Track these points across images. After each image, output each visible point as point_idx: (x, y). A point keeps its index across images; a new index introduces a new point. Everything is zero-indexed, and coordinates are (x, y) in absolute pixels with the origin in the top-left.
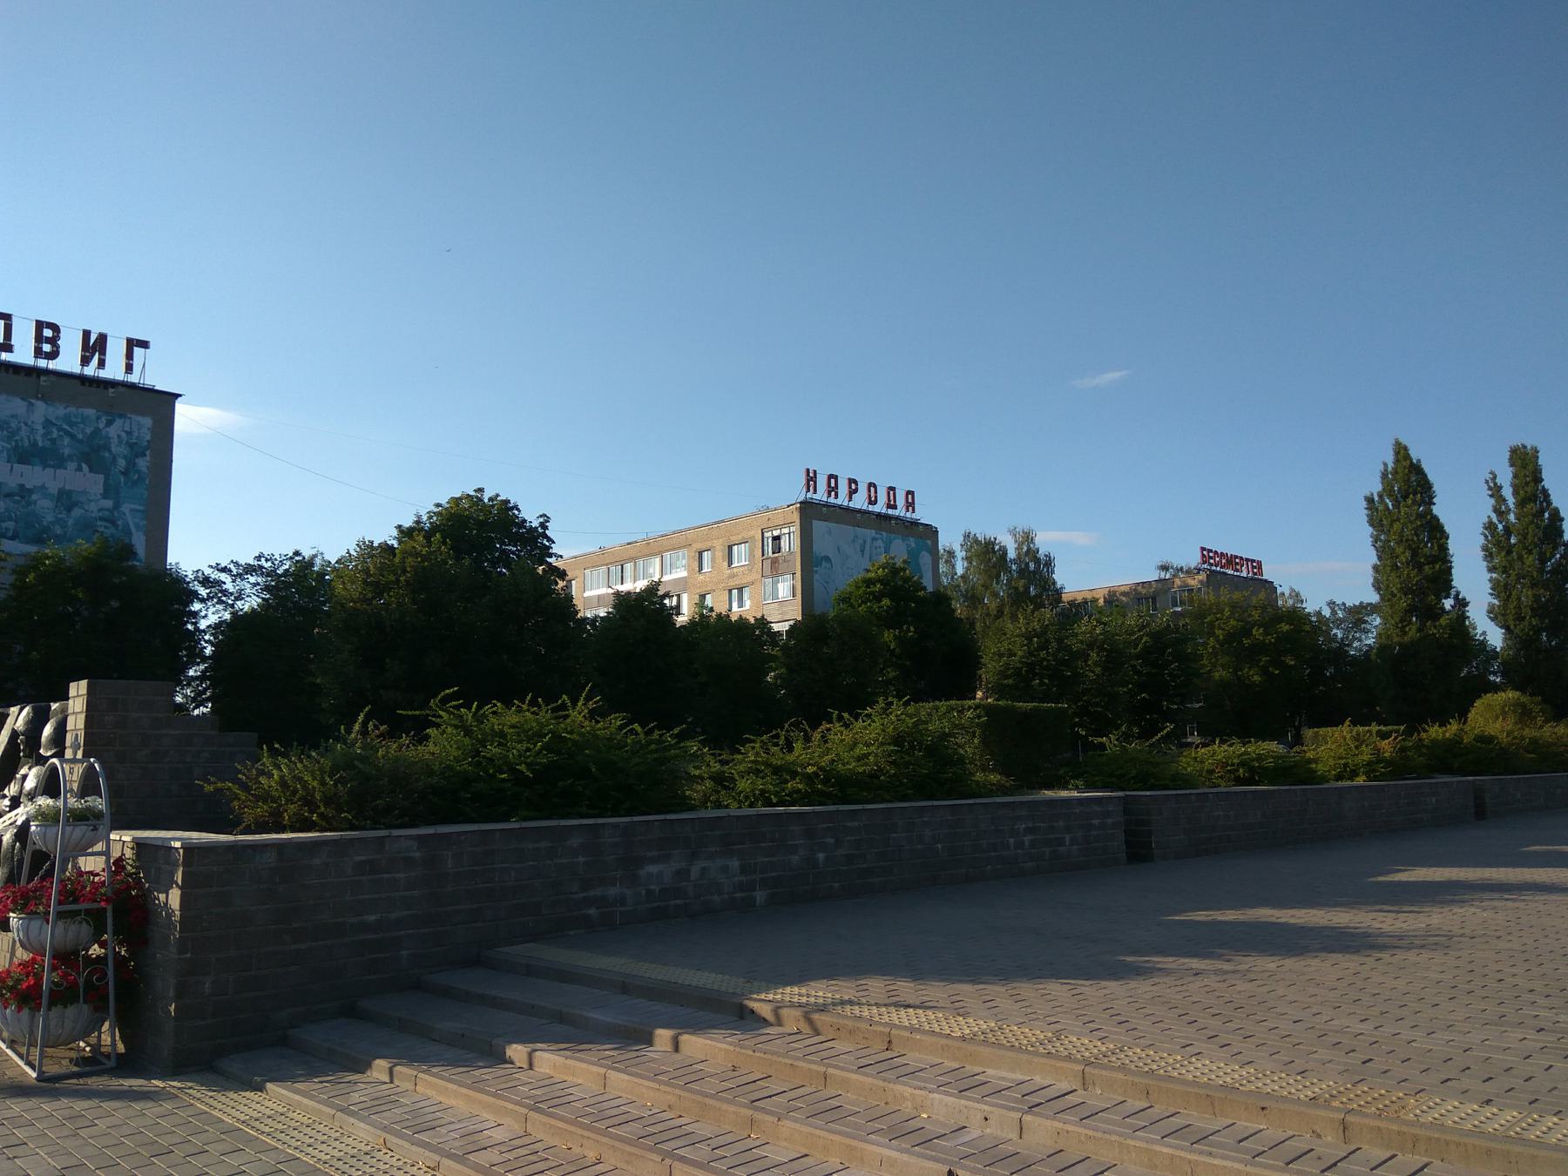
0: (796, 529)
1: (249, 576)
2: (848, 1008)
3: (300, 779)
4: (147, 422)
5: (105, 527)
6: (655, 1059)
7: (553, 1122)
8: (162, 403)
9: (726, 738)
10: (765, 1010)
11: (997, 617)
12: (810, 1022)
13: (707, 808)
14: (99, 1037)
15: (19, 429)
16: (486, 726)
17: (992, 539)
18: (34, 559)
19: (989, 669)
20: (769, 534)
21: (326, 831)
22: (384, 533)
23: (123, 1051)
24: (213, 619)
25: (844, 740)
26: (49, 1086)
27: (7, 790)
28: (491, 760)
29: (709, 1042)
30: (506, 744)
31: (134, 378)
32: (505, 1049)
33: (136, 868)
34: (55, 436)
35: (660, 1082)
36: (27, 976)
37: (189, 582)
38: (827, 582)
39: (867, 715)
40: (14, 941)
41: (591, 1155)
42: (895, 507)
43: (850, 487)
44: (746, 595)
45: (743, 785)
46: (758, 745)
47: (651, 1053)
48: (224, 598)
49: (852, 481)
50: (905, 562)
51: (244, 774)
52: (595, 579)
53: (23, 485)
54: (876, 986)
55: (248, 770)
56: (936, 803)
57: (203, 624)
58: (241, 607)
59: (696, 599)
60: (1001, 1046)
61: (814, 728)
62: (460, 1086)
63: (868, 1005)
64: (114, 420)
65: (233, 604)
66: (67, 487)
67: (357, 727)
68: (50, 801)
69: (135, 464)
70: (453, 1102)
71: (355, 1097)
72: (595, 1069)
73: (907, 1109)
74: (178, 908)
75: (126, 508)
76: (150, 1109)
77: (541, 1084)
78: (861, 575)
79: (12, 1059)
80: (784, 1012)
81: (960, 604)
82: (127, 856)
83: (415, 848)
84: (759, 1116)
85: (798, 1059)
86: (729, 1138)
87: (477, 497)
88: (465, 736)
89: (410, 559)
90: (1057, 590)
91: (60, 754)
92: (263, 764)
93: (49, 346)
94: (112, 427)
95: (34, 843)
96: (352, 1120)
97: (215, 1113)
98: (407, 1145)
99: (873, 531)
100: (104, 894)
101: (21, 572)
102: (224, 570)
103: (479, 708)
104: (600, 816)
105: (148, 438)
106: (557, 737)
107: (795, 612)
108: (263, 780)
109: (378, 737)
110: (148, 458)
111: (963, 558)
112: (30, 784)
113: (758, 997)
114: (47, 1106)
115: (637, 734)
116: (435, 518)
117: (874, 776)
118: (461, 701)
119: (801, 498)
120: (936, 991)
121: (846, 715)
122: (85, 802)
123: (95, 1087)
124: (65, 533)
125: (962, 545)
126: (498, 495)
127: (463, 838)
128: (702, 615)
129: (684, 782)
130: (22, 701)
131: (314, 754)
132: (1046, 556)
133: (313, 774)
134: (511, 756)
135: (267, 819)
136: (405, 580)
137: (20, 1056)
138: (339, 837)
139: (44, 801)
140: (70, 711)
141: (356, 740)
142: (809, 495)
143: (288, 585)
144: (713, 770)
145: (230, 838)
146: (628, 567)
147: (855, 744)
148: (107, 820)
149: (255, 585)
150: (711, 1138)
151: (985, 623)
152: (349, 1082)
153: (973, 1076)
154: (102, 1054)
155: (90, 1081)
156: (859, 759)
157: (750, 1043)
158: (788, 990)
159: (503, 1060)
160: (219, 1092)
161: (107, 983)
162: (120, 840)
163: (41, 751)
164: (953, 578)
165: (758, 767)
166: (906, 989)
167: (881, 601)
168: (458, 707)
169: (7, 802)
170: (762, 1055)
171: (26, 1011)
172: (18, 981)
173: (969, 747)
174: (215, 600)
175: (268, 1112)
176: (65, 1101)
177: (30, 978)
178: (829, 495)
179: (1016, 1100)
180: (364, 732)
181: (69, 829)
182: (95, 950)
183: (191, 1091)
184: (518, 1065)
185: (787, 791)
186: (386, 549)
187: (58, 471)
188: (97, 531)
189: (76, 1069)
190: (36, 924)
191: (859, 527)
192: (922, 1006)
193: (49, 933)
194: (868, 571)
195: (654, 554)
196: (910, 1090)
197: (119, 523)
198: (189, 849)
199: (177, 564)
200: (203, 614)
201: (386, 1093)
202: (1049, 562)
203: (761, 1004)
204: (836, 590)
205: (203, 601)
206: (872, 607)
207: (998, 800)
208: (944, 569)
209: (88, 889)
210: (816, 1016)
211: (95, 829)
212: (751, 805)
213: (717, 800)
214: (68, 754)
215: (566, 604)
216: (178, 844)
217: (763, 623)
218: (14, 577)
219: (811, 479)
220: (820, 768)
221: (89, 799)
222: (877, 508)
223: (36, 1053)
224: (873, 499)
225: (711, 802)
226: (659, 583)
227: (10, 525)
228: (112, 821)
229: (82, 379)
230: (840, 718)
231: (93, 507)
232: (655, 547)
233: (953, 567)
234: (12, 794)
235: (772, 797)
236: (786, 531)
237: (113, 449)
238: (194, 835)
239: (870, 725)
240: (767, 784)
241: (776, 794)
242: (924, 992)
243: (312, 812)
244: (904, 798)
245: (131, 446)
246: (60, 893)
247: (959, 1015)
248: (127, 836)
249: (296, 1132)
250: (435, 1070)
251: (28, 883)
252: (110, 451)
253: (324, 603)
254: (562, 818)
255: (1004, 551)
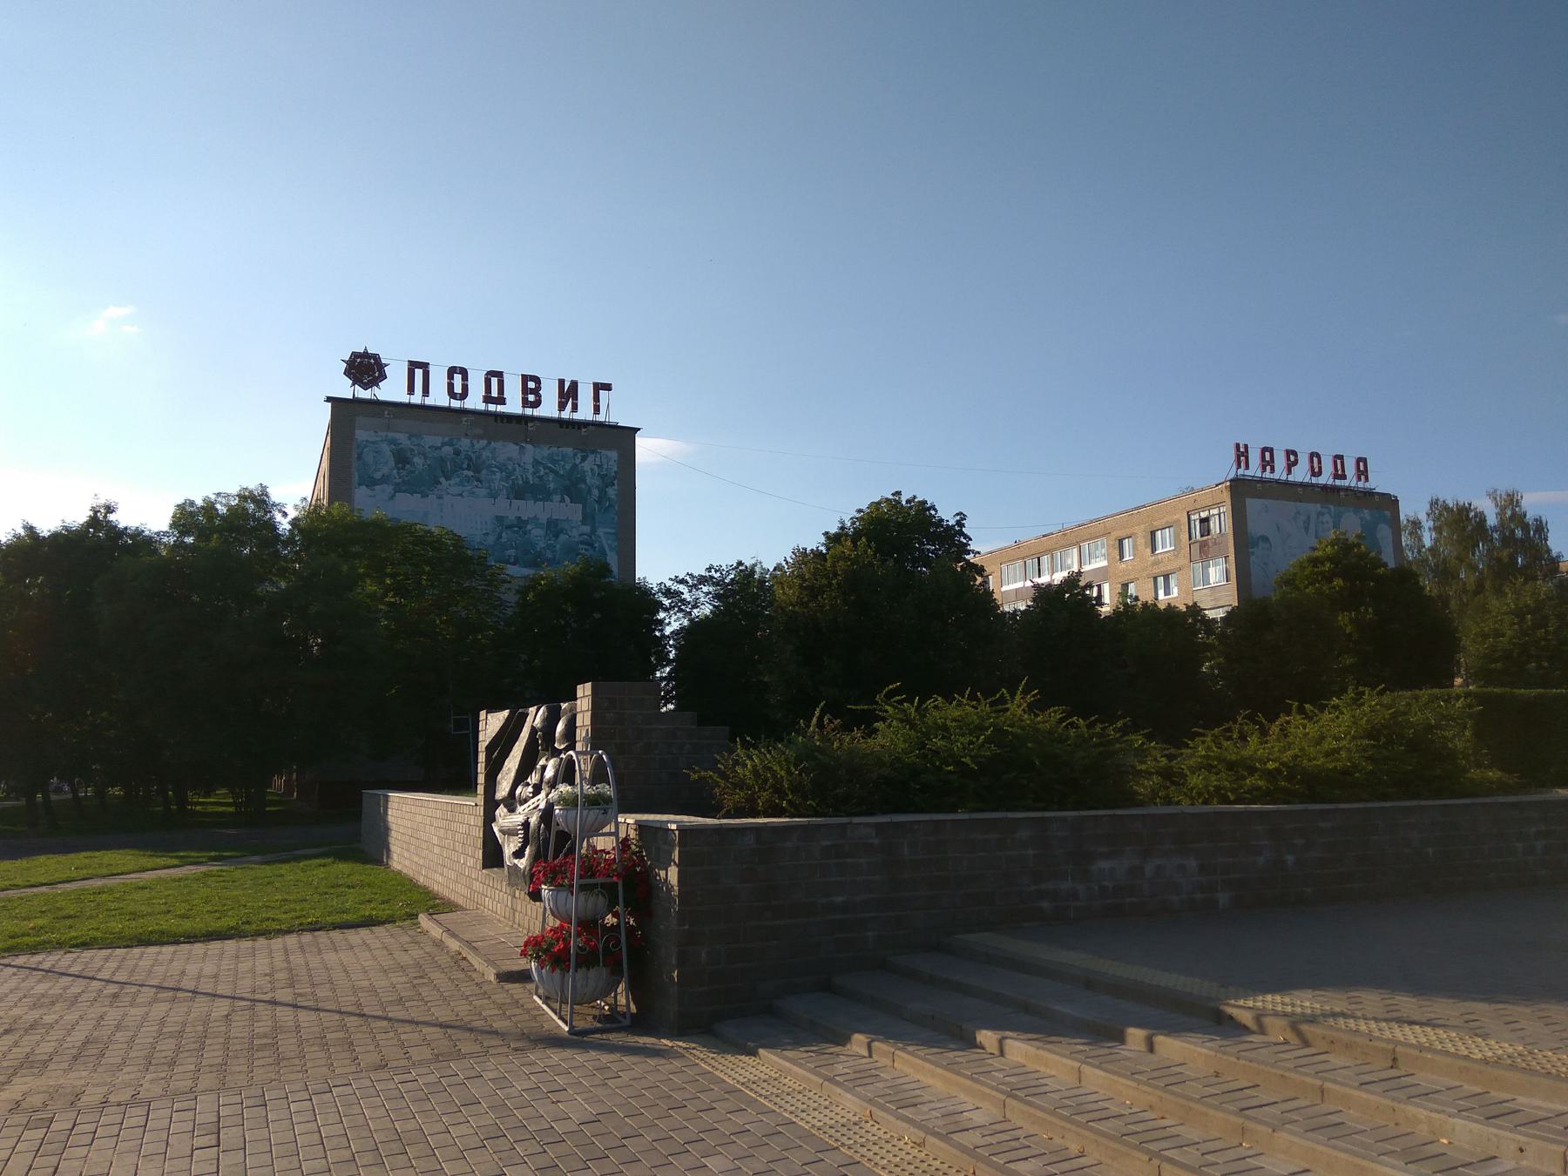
0: (1226, 509)
1: (702, 586)
2: (1341, 1021)
3: (770, 769)
4: (614, 455)
5: (586, 550)
6: (1129, 1058)
7: (1032, 1110)
8: (624, 438)
9: (1174, 734)
10: (1246, 1018)
11: (1476, 593)
12: (1299, 1034)
13: (1155, 804)
14: (615, 997)
15: (515, 470)
16: (929, 720)
17: (1467, 505)
18: (533, 580)
19: (1470, 651)
20: (1197, 516)
21: (795, 817)
22: (814, 541)
23: (635, 1011)
24: (675, 626)
25: (1308, 734)
26: (578, 1039)
27: (529, 778)
28: (936, 752)
29: (1187, 1045)
30: (950, 738)
31: (601, 418)
32: (975, 1034)
33: (640, 847)
34: (542, 473)
35: (1139, 1082)
36: (558, 941)
37: (655, 594)
38: (1265, 564)
39: (1334, 707)
40: (545, 908)
41: (1074, 1148)
42: (1344, 477)
43: (1288, 459)
44: (1172, 583)
45: (1195, 780)
46: (1209, 739)
47: (1122, 1051)
48: (683, 607)
49: (1289, 453)
50: (1359, 536)
51: (722, 764)
52: (1011, 575)
53: (520, 517)
54: (1371, 1000)
55: (726, 761)
56: (1423, 803)
57: (668, 630)
58: (697, 614)
59: (1119, 588)
60: (1533, 1072)
61: (1272, 720)
62: (937, 1066)
63: (1366, 1019)
64: (587, 456)
65: (690, 612)
66: (554, 517)
67: (815, 720)
68: (569, 788)
69: (606, 492)
70: (931, 1081)
71: (839, 1068)
72: (1069, 1062)
73: (1423, 1132)
74: (676, 884)
75: (601, 532)
76: (665, 1066)
77: (1016, 1071)
78: (1305, 555)
79: (547, 1013)
80: (1267, 1021)
81: (1429, 580)
82: (631, 837)
83: (874, 835)
84: (1250, 1125)
85: (1289, 1069)
86: (1218, 1145)
87: (895, 500)
88: (910, 729)
89: (841, 563)
90: (1553, 559)
91: (572, 747)
92: (738, 755)
93: (533, 396)
94: (586, 462)
95: (558, 824)
96: (839, 1090)
97: (717, 1073)
98: (892, 1119)
99: (1319, 505)
100: (615, 870)
101: (523, 592)
102: (682, 582)
103: (921, 702)
104: (1044, 809)
105: (615, 469)
106: (999, 731)
107: (1230, 599)
108: (739, 769)
109: (833, 730)
110: (616, 487)
111: (1430, 529)
112: (549, 773)
113: (1236, 1003)
114: (580, 1057)
115: (1077, 727)
116: (857, 523)
117: (1346, 773)
118: (904, 696)
119: (1232, 476)
120: (1444, 1008)
121: (1308, 706)
122: (597, 788)
123: (616, 1043)
124: (555, 556)
125: (1428, 515)
126: (915, 497)
127: (916, 827)
128: (1126, 605)
129: (1131, 777)
130: (538, 703)
131: (780, 746)
132: (1536, 520)
133: (779, 763)
134: (955, 748)
135: (743, 805)
136: (837, 584)
137: (554, 1011)
138: (807, 823)
139: (564, 788)
140: (578, 710)
141: (814, 732)
142: (1240, 472)
143: (734, 593)
144: (1161, 764)
145: (716, 821)
146: (1045, 559)
147: (1322, 738)
148: (615, 804)
149: (708, 593)
150: (1199, 1143)
151: (1461, 599)
152: (832, 1053)
153: (1501, 1103)
154: (619, 1012)
155: (611, 1036)
156: (1327, 754)
157: (1234, 1050)
158: (1269, 997)
159: (972, 1044)
160: (719, 1054)
161: (621, 949)
162: (625, 822)
163: (556, 745)
164: (1419, 552)
165: (1210, 762)
166: (1407, 1004)
167: (1331, 582)
168: (900, 702)
169: (530, 789)
170: (1247, 1063)
171: (558, 972)
172: (551, 945)
173: (1461, 740)
174: (676, 609)
175: (763, 1076)
176: (593, 1053)
177: (560, 942)
178: (1264, 469)
179: (1557, 1132)
180: (820, 725)
181: (585, 812)
182: (610, 920)
183: (694, 1051)
184: (989, 1051)
185: (1246, 788)
186: (817, 554)
187: (546, 503)
188: (580, 554)
189: (599, 1025)
190: (563, 895)
191: (1301, 502)
192: (1428, 1023)
193: (574, 903)
194: (1314, 549)
195: (1071, 545)
196: (1425, 1113)
197: (596, 545)
198: (684, 831)
199: (645, 578)
200: (667, 621)
201: (867, 1067)
202: (1541, 528)
203: (1241, 1009)
204: (1277, 571)
205: (666, 610)
206: (1321, 588)
207: (1501, 799)
208: (1409, 542)
209: (602, 865)
210: (1304, 1027)
211: (605, 812)
212: (1205, 802)
213: (1167, 796)
214: (579, 747)
215: (986, 600)
216: (674, 827)
217: (1195, 610)
218: (518, 596)
219: (1242, 454)
220: (1283, 764)
221: (599, 786)
222: (1322, 480)
223: (567, 1009)
224: (1316, 470)
225: (1160, 798)
226: (1079, 573)
227: (512, 552)
228: (619, 806)
229: (560, 422)
230: (1301, 710)
231: (575, 533)
232: (1073, 537)
233: (1420, 539)
234: (534, 782)
235: (1229, 794)
236: (1215, 511)
237: (588, 481)
238: (685, 818)
239: (1337, 717)
240: (1224, 780)
241: (1233, 791)
242: (1429, 1009)
243: (782, 799)
244: (1385, 797)
245: (602, 477)
246: (581, 868)
247: (1476, 1035)
248: (631, 819)
249: (790, 1097)
250: (910, 1048)
251: (555, 859)
252: (585, 483)
253: (765, 608)
254: (1009, 810)
255: (1481, 518)
